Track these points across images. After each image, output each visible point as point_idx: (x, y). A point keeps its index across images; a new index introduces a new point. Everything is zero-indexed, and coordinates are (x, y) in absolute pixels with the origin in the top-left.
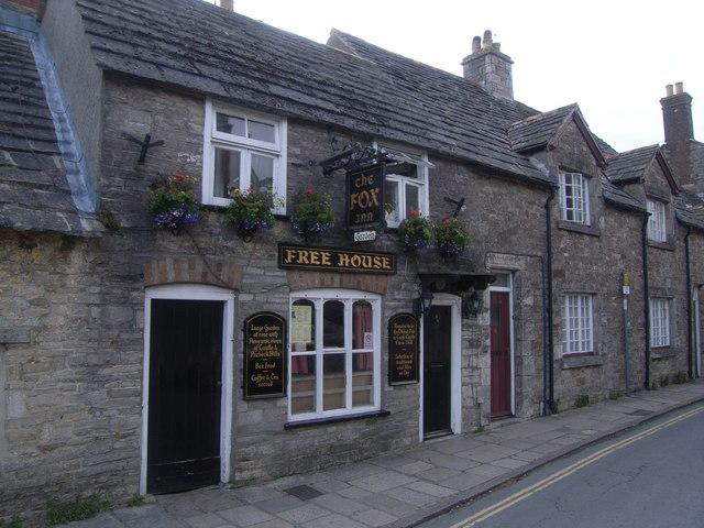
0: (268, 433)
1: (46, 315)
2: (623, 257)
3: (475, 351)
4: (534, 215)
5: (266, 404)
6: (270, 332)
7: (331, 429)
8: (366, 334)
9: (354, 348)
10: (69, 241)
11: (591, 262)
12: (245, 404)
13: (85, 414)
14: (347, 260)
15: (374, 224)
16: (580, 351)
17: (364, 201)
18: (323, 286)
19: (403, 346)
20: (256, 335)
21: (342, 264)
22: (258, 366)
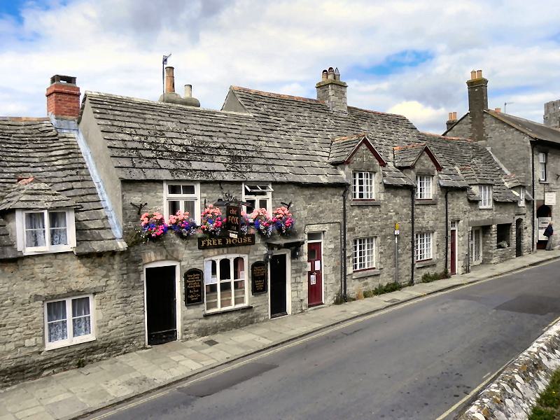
0: (196, 319)
2: (397, 213)
3: (298, 274)
10: (113, 253)
16: (366, 267)
18: (219, 254)
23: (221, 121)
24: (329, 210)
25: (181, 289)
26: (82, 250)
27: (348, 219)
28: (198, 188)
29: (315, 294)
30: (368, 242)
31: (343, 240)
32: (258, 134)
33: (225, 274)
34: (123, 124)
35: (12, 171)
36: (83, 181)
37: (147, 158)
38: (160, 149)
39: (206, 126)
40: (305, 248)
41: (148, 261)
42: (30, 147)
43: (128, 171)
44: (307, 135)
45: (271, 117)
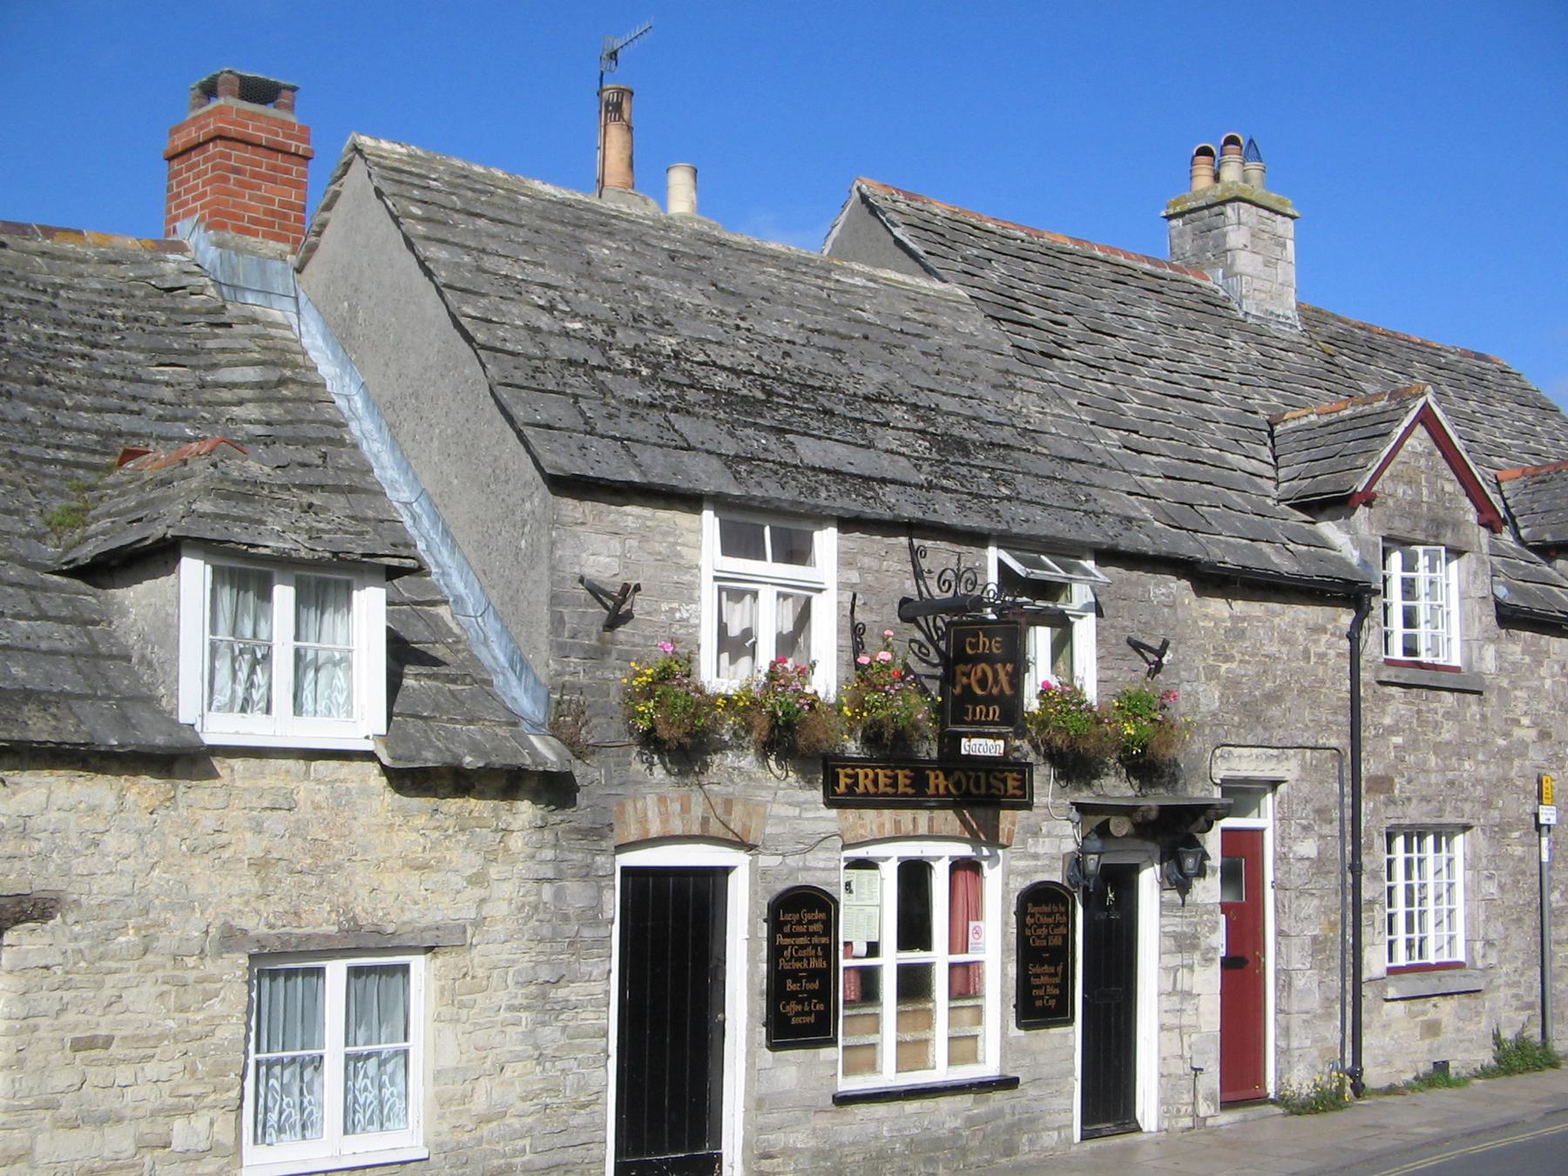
0: (807, 1108)
1: (483, 901)
2: (1544, 735)
4: (1321, 656)
6: (811, 922)
7: (912, 1106)
9: (951, 952)
11: (1459, 750)
13: (530, 1064)
14: (942, 781)
15: (1004, 729)
16: (1431, 958)
17: (982, 682)
19: (1046, 949)
22: (791, 986)
24: (1301, 692)
28: (826, 541)
35: (85, 423)
41: (633, 834)
42: (131, 341)
45: (1031, 309)
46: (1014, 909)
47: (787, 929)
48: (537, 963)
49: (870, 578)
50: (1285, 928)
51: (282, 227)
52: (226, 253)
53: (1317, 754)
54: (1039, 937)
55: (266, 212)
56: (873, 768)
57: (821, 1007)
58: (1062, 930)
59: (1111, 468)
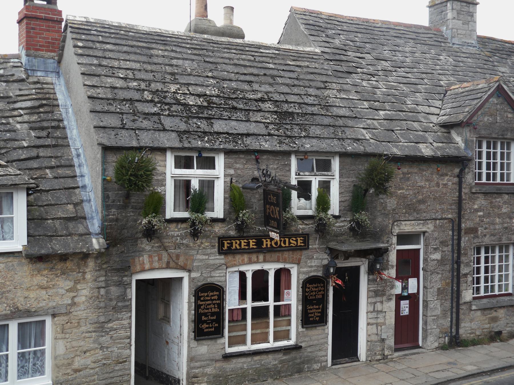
0: (212, 360)
1: (75, 297)
3: (378, 299)
4: (445, 185)
5: (209, 342)
6: (213, 296)
8: (286, 291)
10: (85, 256)
12: (196, 342)
16: (497, 293)
18: (250, 262)
20: (202, 299)
21: (265, 246)
22: (204, 318)
23: (268, 60)
25: (189, 314)
26: (36, 251)
27: (466, 214)
28: (220, 161)
29: (406, 332)
30: (501, 251)
31: (456, 248)
32: (324, 79)
33: (260, 294)
34: (116, 64)
36: (55, 146)
37: (145, 114)
38: (168, 100)
39: (245, 66)
40: (393, 257)
43: (113, 133)
44: (405, 80)
45: (349, 53)
46: (301, 286)
47: (202, 299)
48: (99, 316)
49: (239, 172)
50: (426, 285)
51: (52, 47)
52: (31, 58)
53: (442, 221)
54: (312, 296)
55: (46, 42)
56: (239, 240)
57: (217, 325)
58: (322, 292)
59: (359, 118)
